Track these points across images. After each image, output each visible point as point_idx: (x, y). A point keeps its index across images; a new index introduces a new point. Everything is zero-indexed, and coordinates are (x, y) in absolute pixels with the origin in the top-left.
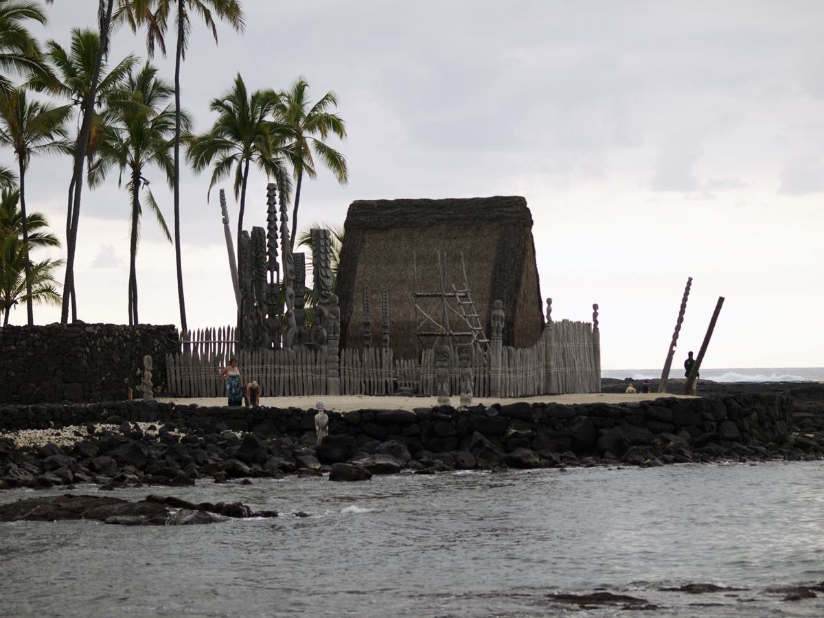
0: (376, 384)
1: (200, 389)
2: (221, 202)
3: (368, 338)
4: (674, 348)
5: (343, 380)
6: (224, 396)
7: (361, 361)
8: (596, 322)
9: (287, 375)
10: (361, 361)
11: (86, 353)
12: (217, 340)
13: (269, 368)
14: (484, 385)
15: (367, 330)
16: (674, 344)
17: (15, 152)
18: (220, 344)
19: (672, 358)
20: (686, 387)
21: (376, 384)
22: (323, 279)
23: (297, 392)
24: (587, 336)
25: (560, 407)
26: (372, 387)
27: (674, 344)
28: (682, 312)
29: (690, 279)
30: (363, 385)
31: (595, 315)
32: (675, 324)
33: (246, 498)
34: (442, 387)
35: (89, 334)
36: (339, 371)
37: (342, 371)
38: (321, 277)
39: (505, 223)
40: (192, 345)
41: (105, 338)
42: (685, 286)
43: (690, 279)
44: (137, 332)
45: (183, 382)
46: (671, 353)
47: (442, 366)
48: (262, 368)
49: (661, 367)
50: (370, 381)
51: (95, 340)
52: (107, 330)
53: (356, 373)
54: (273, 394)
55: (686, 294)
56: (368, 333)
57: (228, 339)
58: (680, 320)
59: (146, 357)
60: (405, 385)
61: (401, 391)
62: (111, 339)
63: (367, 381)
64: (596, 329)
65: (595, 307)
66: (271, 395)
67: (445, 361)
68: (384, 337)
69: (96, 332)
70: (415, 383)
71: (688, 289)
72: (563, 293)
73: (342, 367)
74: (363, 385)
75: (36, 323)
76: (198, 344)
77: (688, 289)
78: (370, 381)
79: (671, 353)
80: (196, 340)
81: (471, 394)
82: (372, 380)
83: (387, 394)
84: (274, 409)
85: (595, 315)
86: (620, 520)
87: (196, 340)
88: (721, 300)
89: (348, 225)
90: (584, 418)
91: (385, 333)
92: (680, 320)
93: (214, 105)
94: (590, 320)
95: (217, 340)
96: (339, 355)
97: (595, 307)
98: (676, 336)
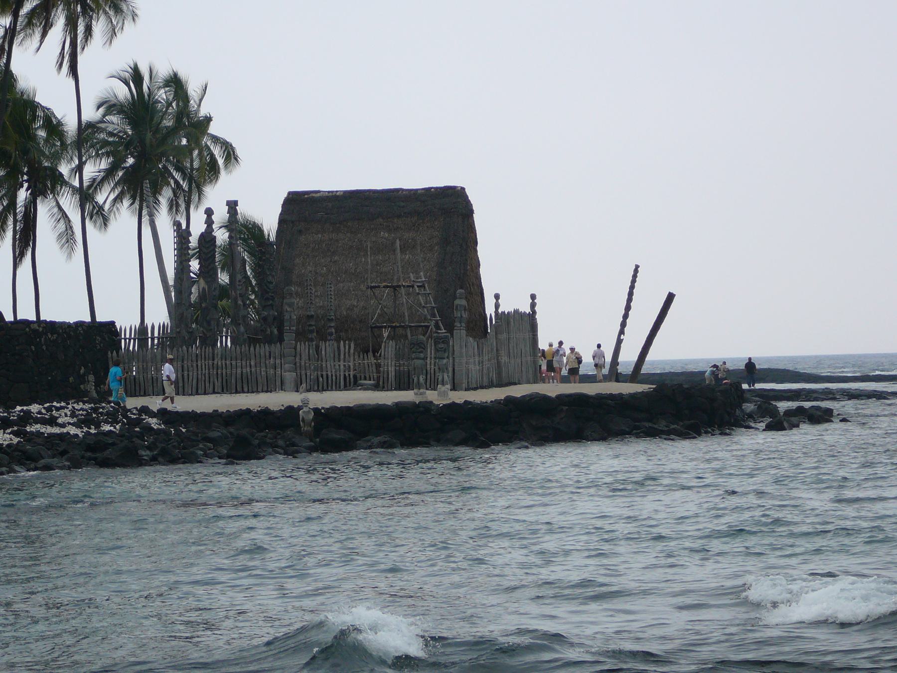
3: (312, 332)
8: (534, 312)
9: (239, 371)
16: (622, 332)
17: (208, 119)
20: (636, 375)
21: (334, 378)
23: (181, 390)
24: (526, 323)
25: (545, 398)
27: (622, 332)
28: (630, 300)
29: (637, 267)
30: (321, 379)
31: (533, 305)
33: (274, 516)
34: (418, 379)
36: (295, 364)
39: (444, 218)
40: (123, 341)
43: (637, 267)
44: (80, 329)
47: (417, 358)
49: (635, 358)
58: (628, 308)
60: (365, 379)
61: (362, 385)
62: (55, 336)
63: (324, 373)
64: (532, 315)
65: (533, 297)
67: (421, 352)
68: (330, 331)
69: (41, 329)
72: (503, 283)
73: (297, 360)
74: (321, 379)
76: (130, 340)
80: (128, 336)
81: (449, 386)
83: (346, 388)
84: (334, 409)
85: (533, 305)
86: (551, 523)
87: (128, 336)
89: (282, 221)
90: (565, 408)
92: (628, 308)
94: (528, 310)
96: (295, 348)
97: (533, 297)
98: (623, 325)
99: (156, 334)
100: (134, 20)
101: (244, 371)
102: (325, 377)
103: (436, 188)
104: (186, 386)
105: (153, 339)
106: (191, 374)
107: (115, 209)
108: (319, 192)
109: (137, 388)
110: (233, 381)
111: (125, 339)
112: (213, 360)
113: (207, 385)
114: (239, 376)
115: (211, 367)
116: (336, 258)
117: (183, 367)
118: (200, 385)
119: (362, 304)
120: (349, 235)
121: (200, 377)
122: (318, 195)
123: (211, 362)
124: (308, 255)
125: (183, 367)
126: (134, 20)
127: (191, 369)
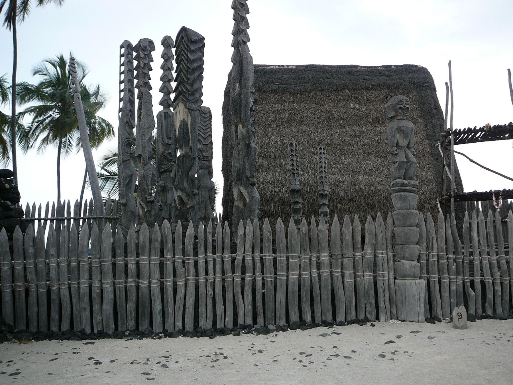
0: (498, 288)
9: (294, 276)
15: (297, 200)
21: (498, 288)
26: (490, 295)
40: (36, 222)
48: (233, 260)
50: (483, 284)
53: (454, 267)
56: (297, 203)
63: (478, 279)
76: (46, 221)
78: (483, 284)
80: (43, 216)
82: (489, 280)
87: (43, 216)
91: (324, 204)
99: (72, 215)
100: (60, 3)
101: (306, 276)
102: (478, 286)
103: (396, 66)
104: (170, 309)
105: (69, 220)
106: (181, 282)
107: (43, 147)
108: (269, 66)
109: (54, 315)
110: (281, 298)
111: (39, 220)
112: (234, 250)
113: (220, 307)
114: (294, 288)
115: (228, 267)
116: (305, 128)
117: (162, 265)
118: (202, 309)
119: (349, 179)
120: (314, 105)
121: (202, 289)
122: (268, 68)
123: (227, 256)
124: (270, 125)
125: (162, 265)
126: (60, 3)
127: (181, 270)
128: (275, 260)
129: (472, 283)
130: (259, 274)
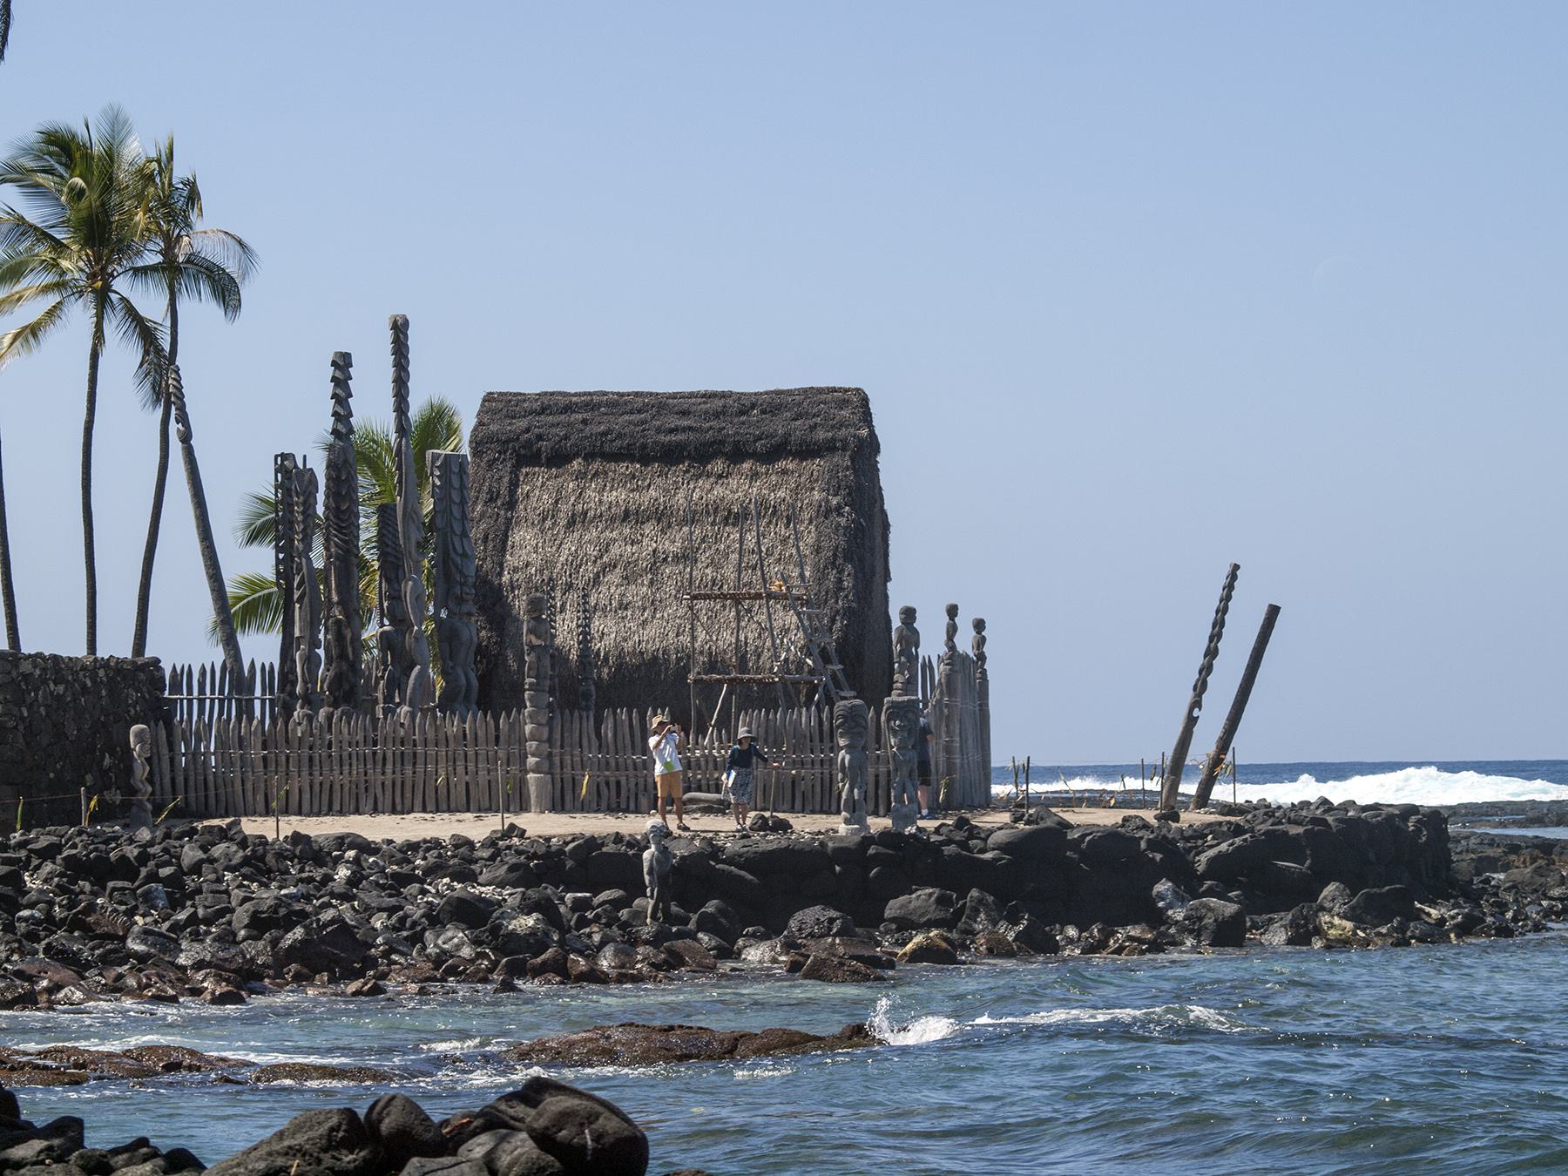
1: (231, 800)
2: (406, 358)
4: (1196, 713)
5: (558, 777)
6: (468, 810)
7: (598, 734)
8: (981, 657)
10: (598, 734)
11: (22, 718)
12: (196, 693)
13: (389, 754)
14: (877, 789)
18: (202, 702)
19: (1191, 733)
22: (458, 559)
32: (1199, 660)
35: (26, 677)
37: (557, 760)
38: (453, 554)
41: (52, 686)
42: (1223, 581)
44: (101, 673)
45: (191, 783)
46: (1191, 721)
48: (375, 753)
51: (36, 690)
52: (55, 666)
54: (399, 808)
55: (1226, 598)
57: (222, 691)
59: (135, 728)
62: (61, 688)
66: (394, 811)
70: (612, 779)
71: (1230, 587)
75: (27, 648)
77: (1230, 587)
79: (1191, 721)
88: (1274, 611)
93: (62, 148)
95: (196, 693)
128: (415, 754)
129: (607, 784)
130: (398, 765)
